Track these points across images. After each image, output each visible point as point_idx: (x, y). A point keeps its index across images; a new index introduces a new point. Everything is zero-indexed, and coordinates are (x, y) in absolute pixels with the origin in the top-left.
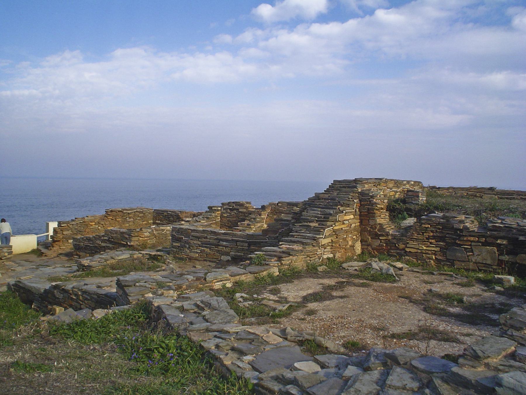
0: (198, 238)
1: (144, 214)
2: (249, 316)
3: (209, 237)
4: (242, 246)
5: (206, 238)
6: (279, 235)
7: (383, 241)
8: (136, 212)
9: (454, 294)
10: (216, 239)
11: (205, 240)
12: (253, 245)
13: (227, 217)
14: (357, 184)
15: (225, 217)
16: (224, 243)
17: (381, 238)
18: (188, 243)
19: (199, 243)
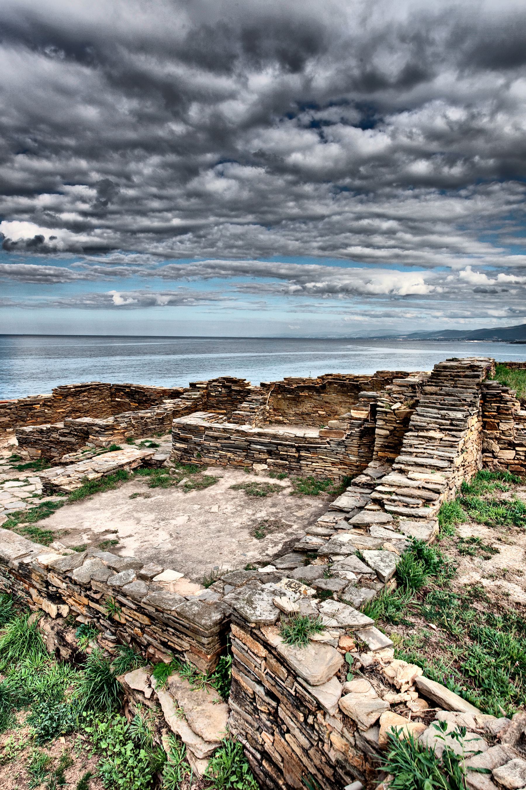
0: (216, 438)
1: (100, 390)
2: (35, 608)
3: (233, 437)
4: (286, 452)
5: (229, 438)
6: (346, 438)
7: (521, 453)
8: (92, 388)
9: (353, 289)
10: (246, 441)
11: (227, 441)
12: (304, 451)
13: (215, 396)
14: (115, 647)
15: (213, 396)
16: (259, 447)
17: (517, 449)
18: (199, 445)
19: (219, 445)
